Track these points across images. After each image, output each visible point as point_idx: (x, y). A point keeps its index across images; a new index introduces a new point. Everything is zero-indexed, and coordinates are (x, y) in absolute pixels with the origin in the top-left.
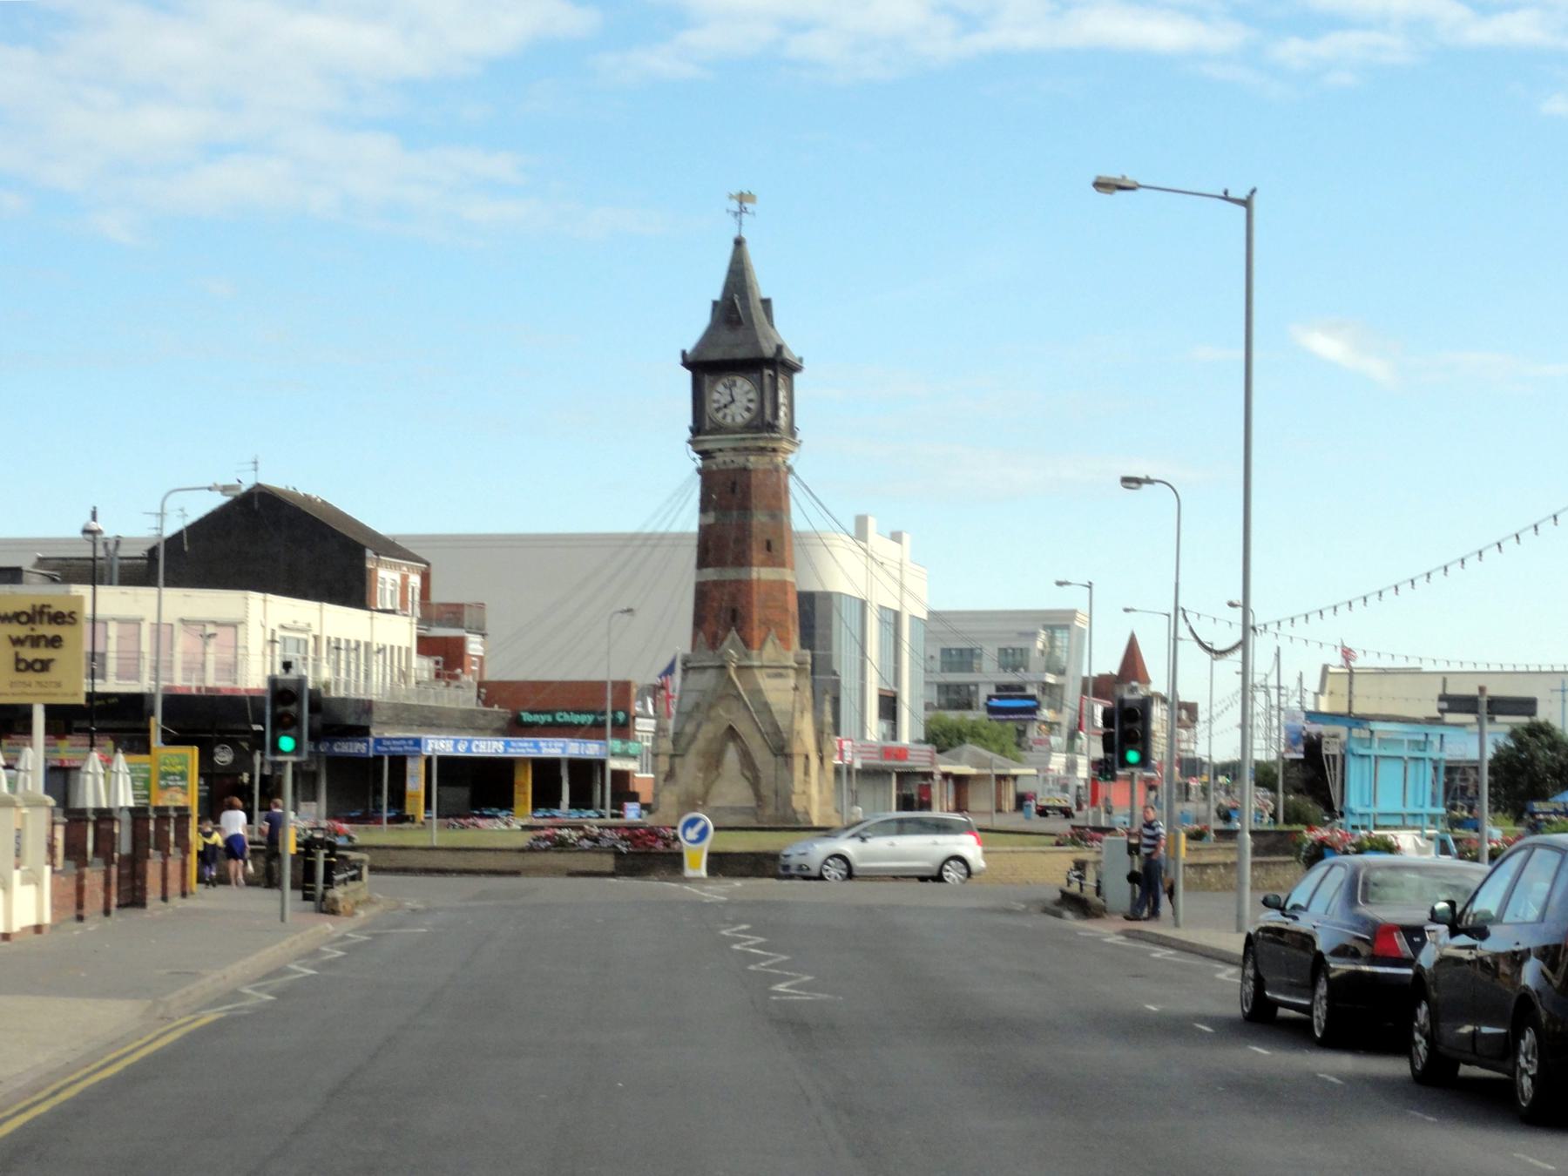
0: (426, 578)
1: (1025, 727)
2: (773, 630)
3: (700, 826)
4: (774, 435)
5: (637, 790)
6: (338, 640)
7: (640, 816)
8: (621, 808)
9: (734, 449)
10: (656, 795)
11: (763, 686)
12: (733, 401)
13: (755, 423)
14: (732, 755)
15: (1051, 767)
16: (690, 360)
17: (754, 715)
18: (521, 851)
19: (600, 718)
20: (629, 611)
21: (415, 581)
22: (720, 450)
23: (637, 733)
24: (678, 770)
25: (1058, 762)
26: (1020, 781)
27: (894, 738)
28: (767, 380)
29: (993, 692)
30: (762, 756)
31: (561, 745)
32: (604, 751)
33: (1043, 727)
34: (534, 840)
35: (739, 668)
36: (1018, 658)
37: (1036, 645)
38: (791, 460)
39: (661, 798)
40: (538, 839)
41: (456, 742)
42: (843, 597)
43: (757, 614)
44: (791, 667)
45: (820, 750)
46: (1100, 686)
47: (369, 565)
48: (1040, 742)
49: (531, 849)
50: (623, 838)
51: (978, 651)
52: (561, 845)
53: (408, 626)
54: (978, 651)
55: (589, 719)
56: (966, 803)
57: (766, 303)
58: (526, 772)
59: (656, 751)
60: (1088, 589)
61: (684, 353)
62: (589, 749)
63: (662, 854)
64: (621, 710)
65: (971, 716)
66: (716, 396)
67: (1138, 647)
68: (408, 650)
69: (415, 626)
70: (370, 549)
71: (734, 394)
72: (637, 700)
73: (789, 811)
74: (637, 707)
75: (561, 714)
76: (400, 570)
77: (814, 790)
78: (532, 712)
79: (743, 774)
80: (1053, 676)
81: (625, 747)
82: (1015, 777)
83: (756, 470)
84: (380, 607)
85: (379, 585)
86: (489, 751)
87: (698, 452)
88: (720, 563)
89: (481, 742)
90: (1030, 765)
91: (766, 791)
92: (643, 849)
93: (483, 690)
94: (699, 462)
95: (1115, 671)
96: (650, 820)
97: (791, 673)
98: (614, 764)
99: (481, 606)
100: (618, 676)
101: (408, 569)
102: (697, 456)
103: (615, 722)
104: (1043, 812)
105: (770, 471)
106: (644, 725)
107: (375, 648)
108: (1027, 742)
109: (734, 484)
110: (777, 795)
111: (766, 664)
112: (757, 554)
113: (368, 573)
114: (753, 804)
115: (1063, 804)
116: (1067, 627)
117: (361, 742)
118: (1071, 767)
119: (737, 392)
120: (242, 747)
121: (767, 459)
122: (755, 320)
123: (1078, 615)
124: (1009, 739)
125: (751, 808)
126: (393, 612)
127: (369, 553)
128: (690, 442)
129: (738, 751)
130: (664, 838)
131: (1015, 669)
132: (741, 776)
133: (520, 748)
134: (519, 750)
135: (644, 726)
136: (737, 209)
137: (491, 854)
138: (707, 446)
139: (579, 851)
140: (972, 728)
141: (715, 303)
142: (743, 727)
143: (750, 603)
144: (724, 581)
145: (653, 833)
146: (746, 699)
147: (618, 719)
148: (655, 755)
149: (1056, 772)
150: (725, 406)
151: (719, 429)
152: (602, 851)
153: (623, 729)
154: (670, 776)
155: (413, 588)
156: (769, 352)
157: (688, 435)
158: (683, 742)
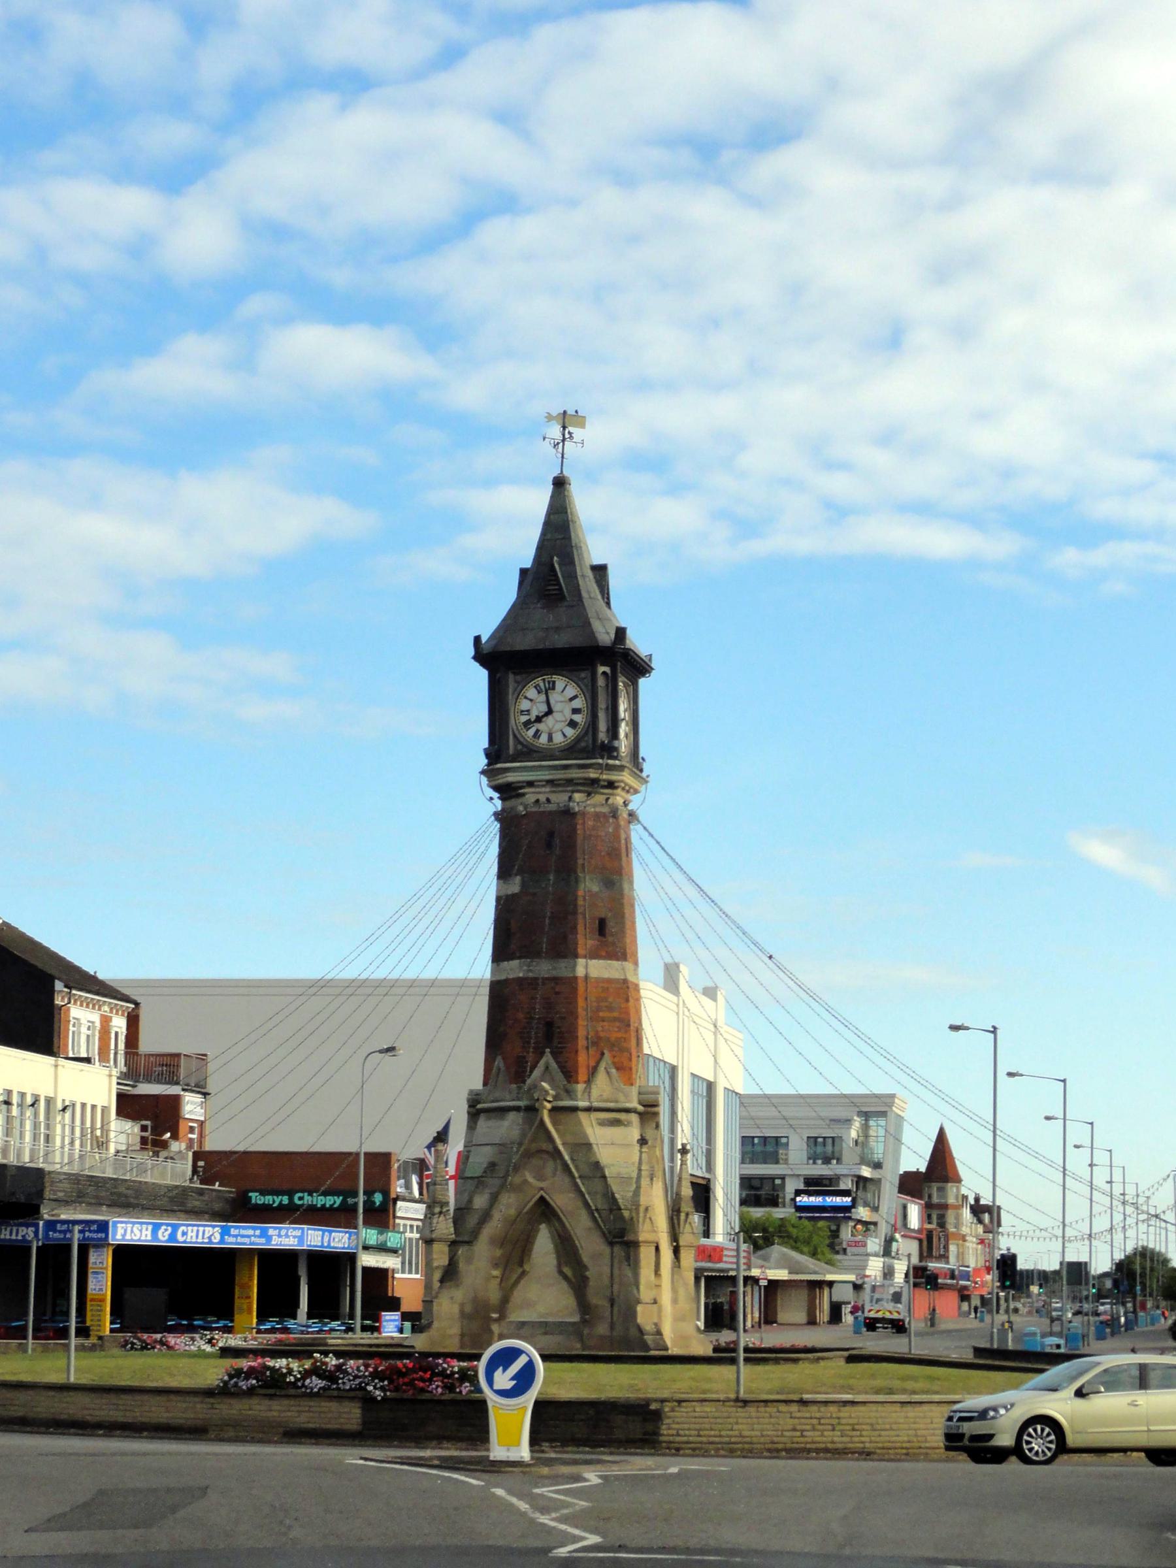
0: (133, 1021)
1: (838, 1227)
2: (607, 1054)
3: (521, 1361)
4: (611, 762)
5: (397, 1294)
6: (9, 1093)
7: (401, 1331)
8: (377, 1319)
9: (550, 782)
10: (428, 1303)
11: (592, 1140)
12: (550, 712)
13: (583, 744)
14: (544, 1243)
15: (868, 1273)
16: (486, 649)
17: (578, 1181)
18: (209, 1393)
19: (350, 1201)
20: (390, 1049)
21: (119, 1024)
22: (530, 784)
23: (397, 1221)
24: (462, 1265)
25: (875, 1267)
26: (835, 1287)
27: (707, 1234)
28: (601, 682)
29: (802, 1187)
30: (590, 1244)
31: (299, 1233)
32: (353, 1244)
33: (859, 1227)
34: (231, 1377)
35: (554, 1110)
36: (829, 1148)
37: (850, 1134)
38: (635, 803)
39: (435, 1308)
40: (237, 1373)
41: (156, 1228)
42: (651, 1060)
43: (583, 1030)
44: (634, 1111)
45: (674, 1237)
46: (911, 1184)
47: (58, 1001)
48: (856, 1244)
49: (224, 1391)
50: (376, 1375)
51: (784, 1140)
52: (274, 1384)
53: (107, 1079)
54: (784, 1140)
55: (334, 1201)
56: (776, 1313)
57: (600, 571)
58: (251, 1269)
59: (428, 1235)
60: (992, 1035)
61: (477, 639)
62: (338, 1240)
63: (440, 1402)
64: (380, 1192)
65: (778, 1213)
66: (525, 705)
67: (947, 1141)
68: (105, 1110)
69: (114, 1080)
70: (59, 979)
71: (552, 702)
72: (399, 1179)
73: (633, 1332)
74: (398, 1188)
75: (300, 1195)
76: (99, 1009)
77: (666, 1298)
78: (263, 1193)
79: (561, 1272)
80: (870, 1170)
81: (382, 1238)
82: (831, 1284)
83: (584, 814)
84: (71, 1055)
85: (71, 1029)
86: (200, 1240)
87: (496, 788)
88: (529, 952)
89: (190, 1228)
90: (847, 1270)
91: (596, 1299)
92: (409, 1394)
93: (201, 1163)
94: (498, 805)
95: (923, 1169)
96: (420, 1342)
97: (634, 1118)
98: (368, 1260)
99: (202, 1057)
100: (375, 1145)
101: (111, 1009)
102: (496, 795)
103: (369, 1206)
104: (871, 1325)
105: (605, 816)
106: (407, 1211)
107: (60, 1106)
108: (841, 1243)
109: (551, 834)
110: (612, 1305)
111: (596, 1104)
112: (585, 940)
113: (56, 1012)
114: (576, 1318)
115: (895, 1316)
116: (883, 1114)
117: (27, 1226)
118: (888, 1273)
119: (554, 697)
120: (496, 1313)
121: (598, 799)
122: (584, 594)
123: (896, 1100)
124: (821, 1240)
125: (574, 1324)
126: (87, 1060)
127: (59, 985)
128: (483, 772)
129: (553, 1238)
130: (443, 1374)
131: (827, 1161)
132: (557, 1275)
133: (243, 1236)
134: (239, 1240)
135: (409, 1212)
136: (559, 437)
137: (162, 1399)
138: (511, 778)
139: (305, 1395)
140: (781, 1226)
141: (523, 572)
142: (562, 1200)
143: (574, 1014)
144: (536, 979)
145: (426, 1361)
146: (567, 1157)
147: (374, 1203)
148: (429, 1242)
149: (873, 1277)
150: (539, 719)
151: (528, 752)
152: (341, 1396)
153: (381, 1216)
154: (450, 1274)
155: (117, 1034)
156: (605, 637)
157: (484, 761)
158: (472, 1221)
